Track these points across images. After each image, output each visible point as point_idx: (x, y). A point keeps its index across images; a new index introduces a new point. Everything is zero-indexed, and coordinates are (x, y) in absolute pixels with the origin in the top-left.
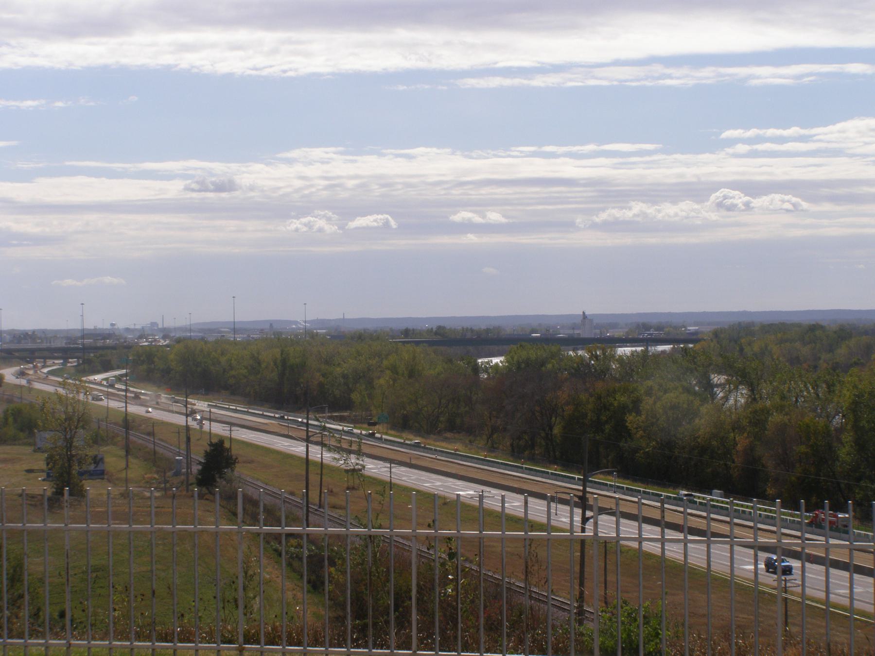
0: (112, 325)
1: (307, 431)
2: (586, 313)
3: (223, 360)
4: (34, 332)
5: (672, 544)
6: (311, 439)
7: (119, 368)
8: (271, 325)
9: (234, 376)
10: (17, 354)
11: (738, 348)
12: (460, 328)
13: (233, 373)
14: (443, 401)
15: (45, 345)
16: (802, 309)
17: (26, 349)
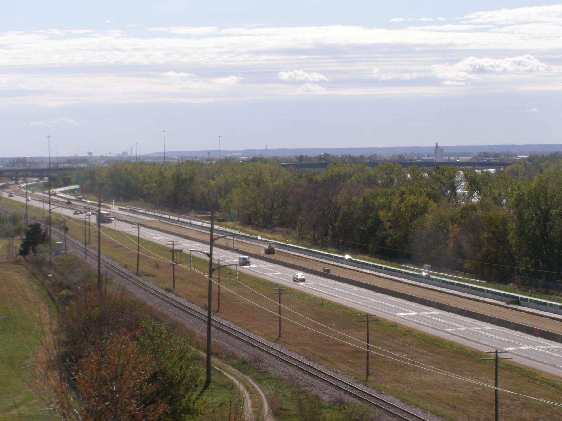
0: (90, 153)
1: (212, 235)
2: (439, 145)
3: (140, 176)
4: (24, 158)
5: (220, 250)
6: (216, 242)
7: (76, 183)
8: (209, 153)
9: (147, 188)
10: (5, 174)
11: (491, 169)
12: (340, 156)
13: (146, 186)
14: (276, 205)
15: (32, 167)
16: (292, 148)
17: (15, 171)
